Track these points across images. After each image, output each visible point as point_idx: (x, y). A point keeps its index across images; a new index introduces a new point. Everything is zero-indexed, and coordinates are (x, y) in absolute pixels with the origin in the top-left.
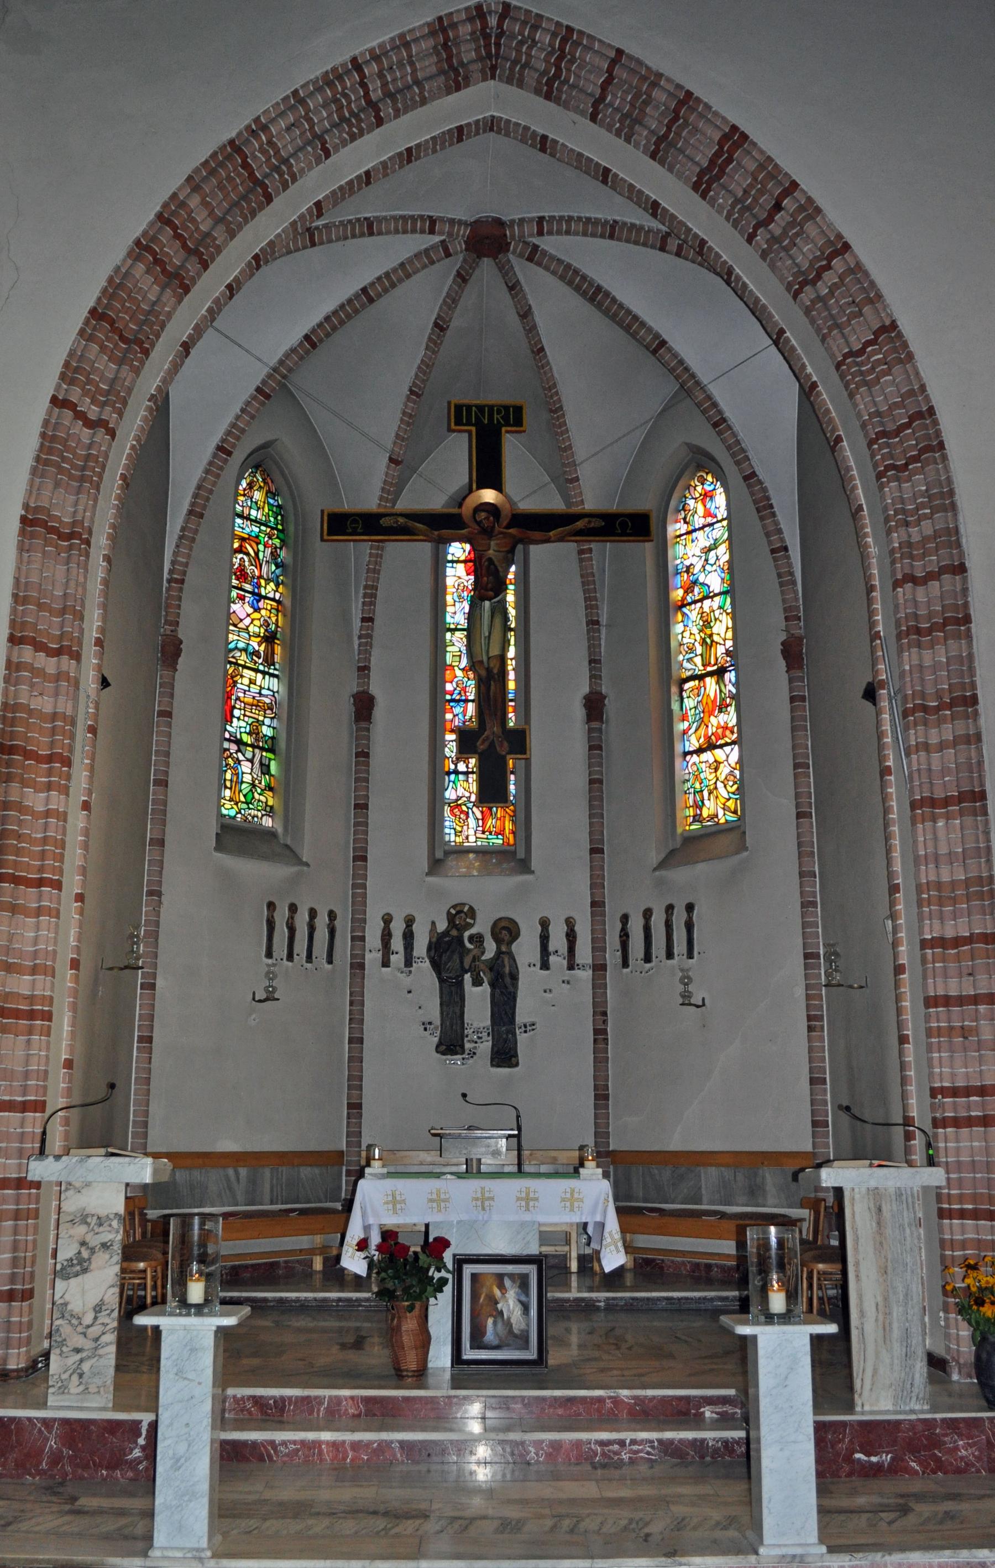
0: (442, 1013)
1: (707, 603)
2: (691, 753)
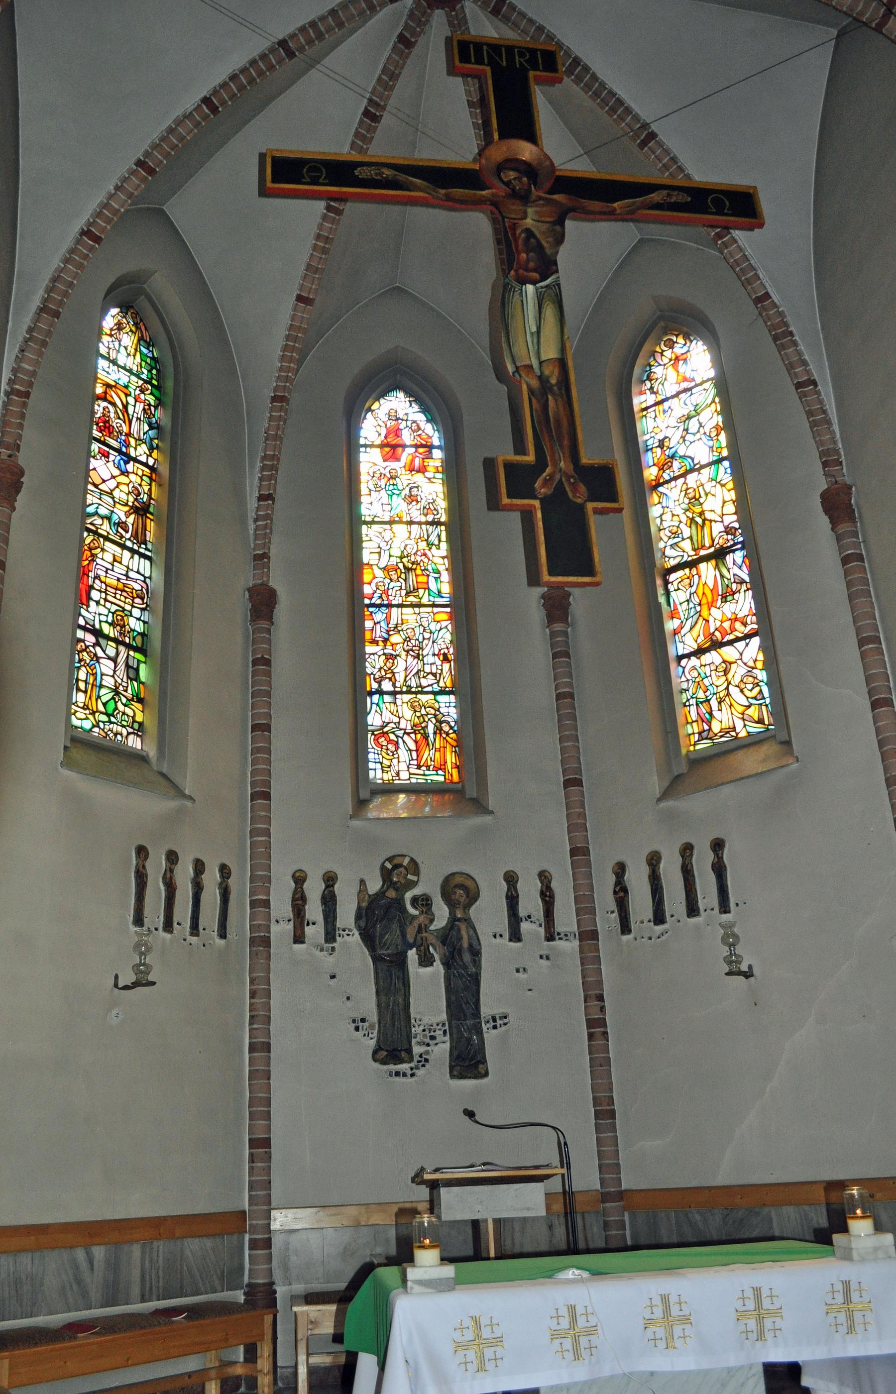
0: (379, 1005)
1: (692, 479)
2: (688, 656)
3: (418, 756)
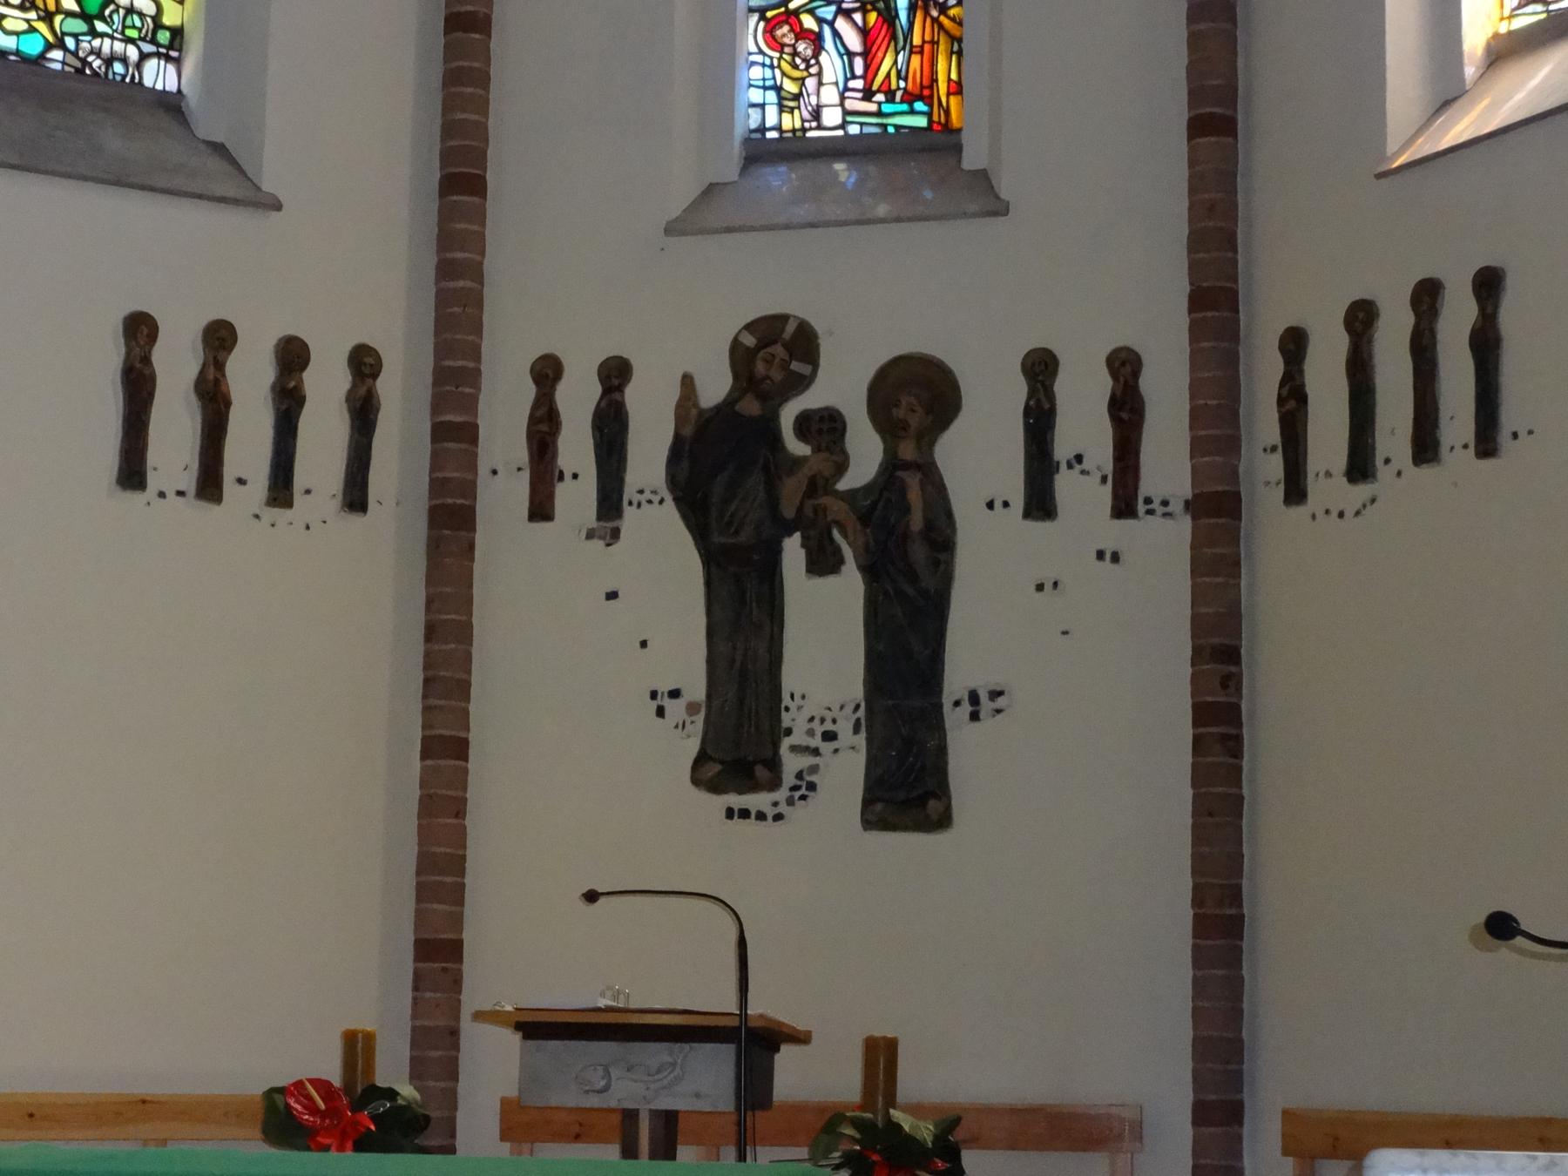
3: (867, 67)
